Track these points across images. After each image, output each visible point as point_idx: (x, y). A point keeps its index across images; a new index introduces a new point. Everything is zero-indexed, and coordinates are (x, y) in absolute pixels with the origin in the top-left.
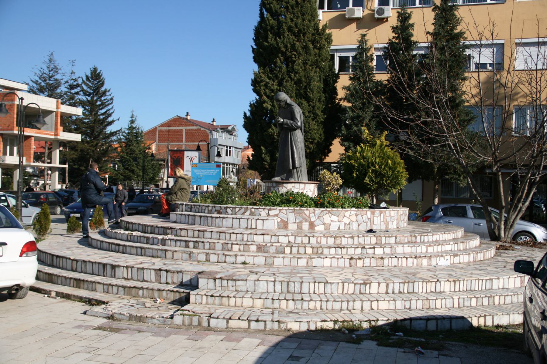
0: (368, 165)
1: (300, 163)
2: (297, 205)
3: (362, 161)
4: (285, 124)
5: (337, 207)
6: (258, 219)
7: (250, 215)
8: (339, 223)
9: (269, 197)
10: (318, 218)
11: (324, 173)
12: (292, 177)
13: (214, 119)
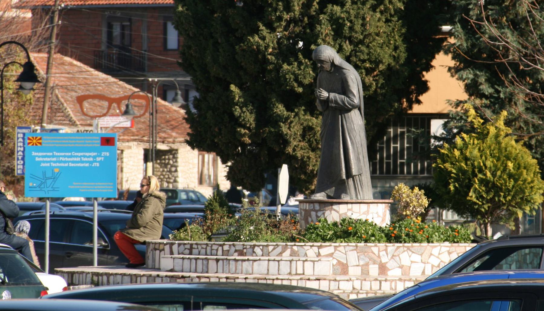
0: (473, 171)
1: (360, 169)
2: (360, 239)
3: (463, 164)
4: (332, 102)
5: (421, 242)
6: (306, 260)
7: (291, 255)
8: (423, 265)
11: (400, 189)
12: (346, 193)
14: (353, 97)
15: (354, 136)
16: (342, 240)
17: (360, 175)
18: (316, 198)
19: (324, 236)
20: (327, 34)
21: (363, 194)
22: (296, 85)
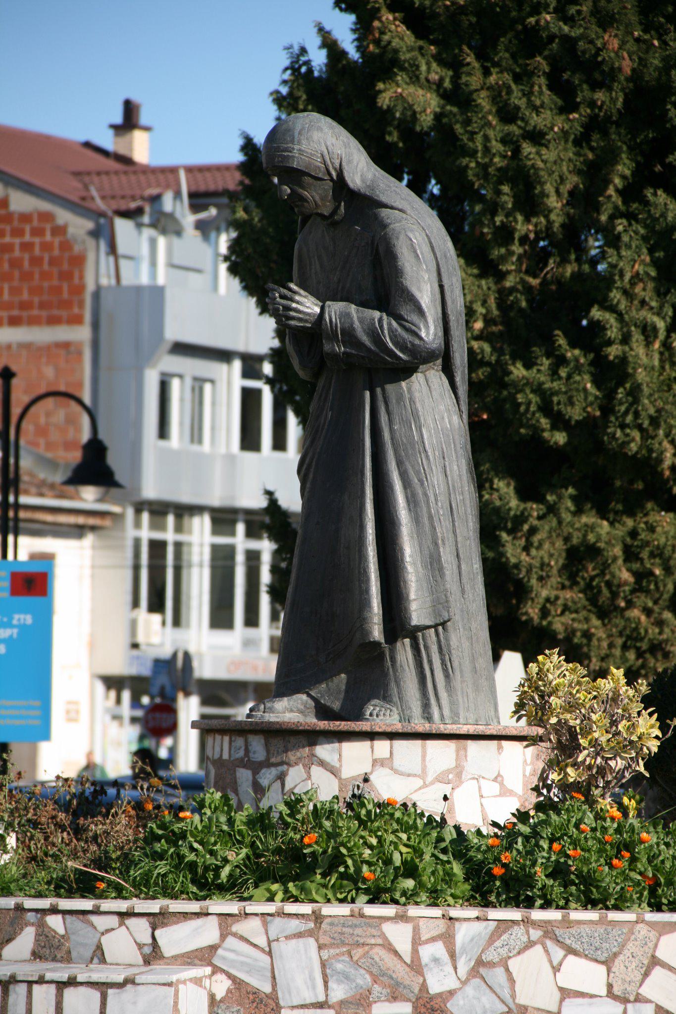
1: (439, 602)
4: (333, 336)
6: (72, 982)
7: (36, 955)
9: (176, 838)
10: (474, 972)
12: (386, 698)
13: (130, 110)
14: (414, 317)
15: (418, 473)
16: (275, 887)
17: (443, 624)
18: (271, 718)
19: (207, 868)
20: (638, 274)
21: (453, 703)
22: (544, 422)
